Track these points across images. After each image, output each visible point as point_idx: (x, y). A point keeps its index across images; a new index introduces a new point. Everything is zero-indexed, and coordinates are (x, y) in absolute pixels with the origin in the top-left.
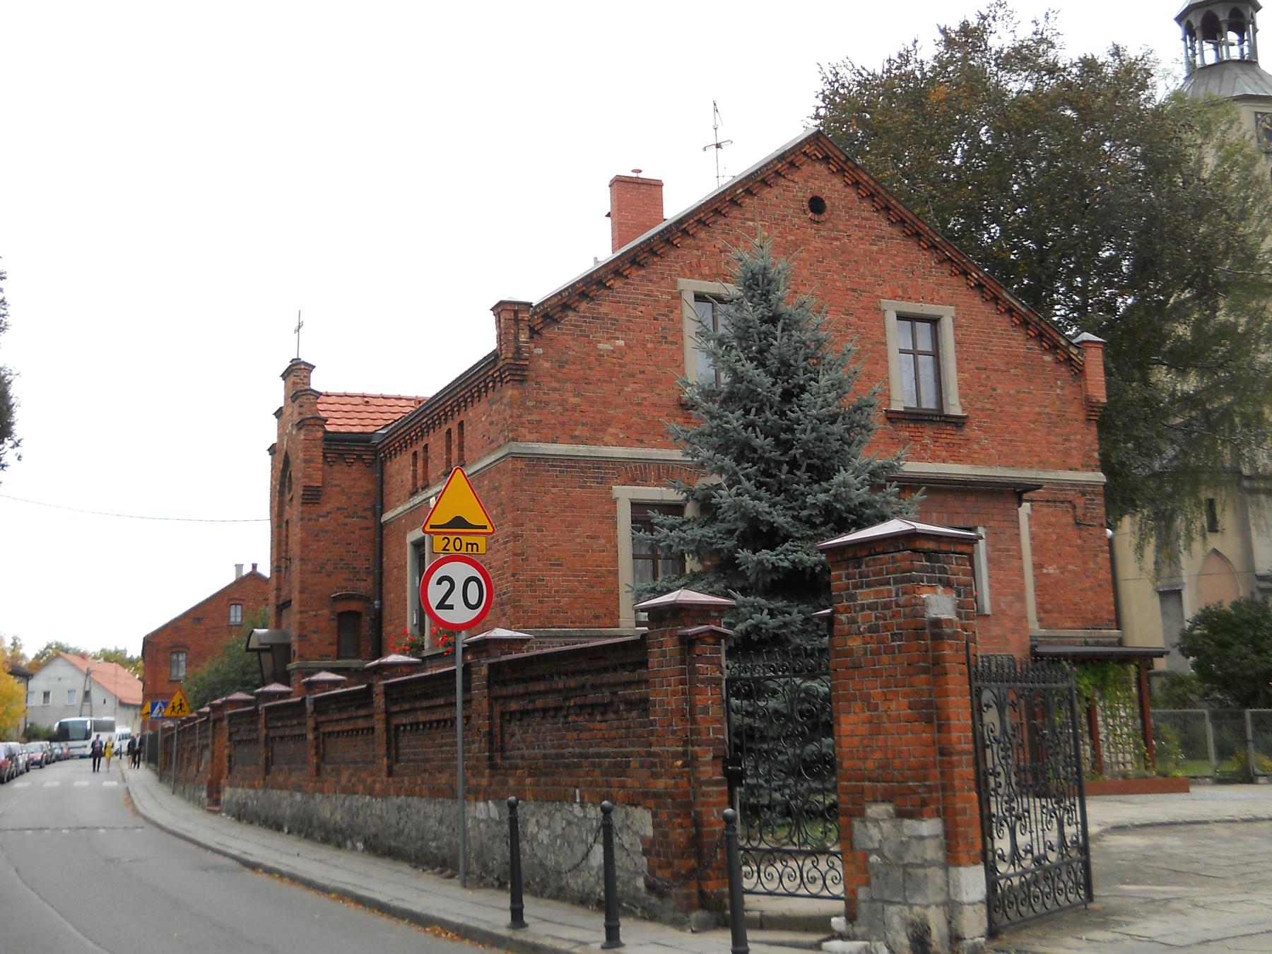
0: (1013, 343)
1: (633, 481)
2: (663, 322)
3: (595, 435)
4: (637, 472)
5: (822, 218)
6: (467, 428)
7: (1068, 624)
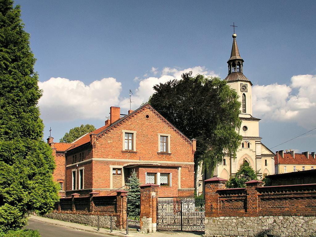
0: (180, 141)
1: (113, 164)
2: (119, 137)
3: (107, 156)
4: (114, 163)
5: (148, 119)
6: (84, 154)
7: (186, 187)
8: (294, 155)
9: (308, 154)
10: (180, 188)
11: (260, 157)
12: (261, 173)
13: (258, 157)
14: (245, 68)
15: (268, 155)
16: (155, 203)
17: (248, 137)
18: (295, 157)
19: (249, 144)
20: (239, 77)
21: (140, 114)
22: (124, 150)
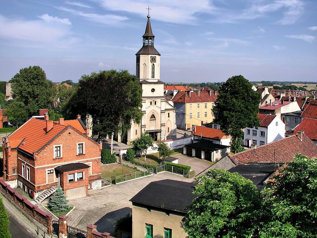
1: (48, 168)
4: (48, 167)
10: (91, 175)
13: (162, 112)
16: (66, 227)
19: (155, 102)
21: (65, 133)
22: (54, 158)
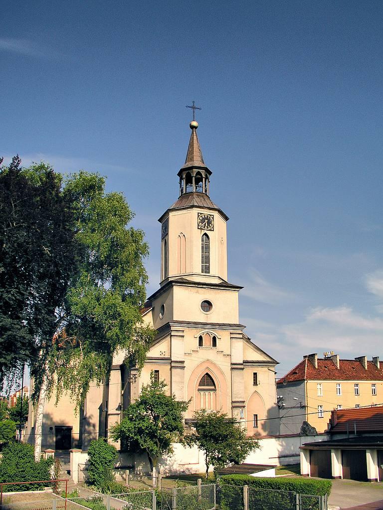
8: (338, 363)
9: (366, 361)
11: (242, 367)
12: (244, 402)
13: (235, 367)
14: (212, 186)
15: (264, 362)
17: (213, 324)
18: (340, 366)
19: (214, 339)
20: (196, 201)
